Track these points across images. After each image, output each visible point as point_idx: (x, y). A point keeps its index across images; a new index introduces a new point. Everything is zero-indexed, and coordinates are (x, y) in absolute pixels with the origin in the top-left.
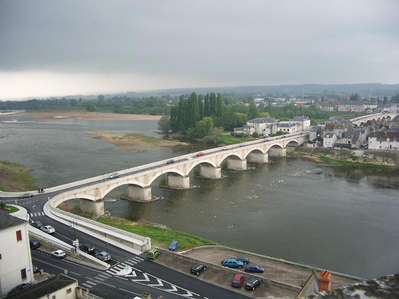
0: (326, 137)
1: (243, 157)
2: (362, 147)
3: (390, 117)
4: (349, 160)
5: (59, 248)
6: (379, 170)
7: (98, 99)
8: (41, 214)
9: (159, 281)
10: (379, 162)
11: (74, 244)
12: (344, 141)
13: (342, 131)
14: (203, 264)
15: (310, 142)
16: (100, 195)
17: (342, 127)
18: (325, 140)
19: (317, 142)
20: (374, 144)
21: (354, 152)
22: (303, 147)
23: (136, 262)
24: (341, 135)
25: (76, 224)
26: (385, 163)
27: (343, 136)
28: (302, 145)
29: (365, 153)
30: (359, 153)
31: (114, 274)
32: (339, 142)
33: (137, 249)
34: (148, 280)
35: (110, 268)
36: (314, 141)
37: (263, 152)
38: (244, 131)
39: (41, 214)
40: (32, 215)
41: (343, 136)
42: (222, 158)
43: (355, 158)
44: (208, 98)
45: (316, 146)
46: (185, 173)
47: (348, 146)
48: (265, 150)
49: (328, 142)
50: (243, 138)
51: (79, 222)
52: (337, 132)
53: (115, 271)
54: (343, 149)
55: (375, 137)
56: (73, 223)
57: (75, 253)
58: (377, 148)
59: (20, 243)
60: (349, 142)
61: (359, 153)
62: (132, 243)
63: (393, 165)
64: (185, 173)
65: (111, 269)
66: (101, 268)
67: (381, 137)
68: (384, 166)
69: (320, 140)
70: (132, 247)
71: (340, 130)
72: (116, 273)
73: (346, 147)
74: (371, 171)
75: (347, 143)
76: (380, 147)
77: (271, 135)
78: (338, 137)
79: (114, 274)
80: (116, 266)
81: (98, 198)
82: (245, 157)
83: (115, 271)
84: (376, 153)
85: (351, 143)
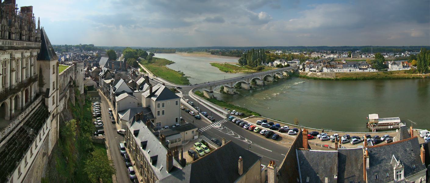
0: (306, 67)
2: (320, 71)
5: (192, 111)
7: (99, 48)
9: (239, 136)
22: (297, 72)
23: (216, 123)
25: (200, 101)
31: (213, 127)
34: (233, 134)
35: (212, 123)
39: (188, 95)
40: (184, 95)
51: (201, 100)
53: (214, 125)
56: (199, 100)
59: (177, 105)
61: (319, 74)
62: (223, 113)
64: (248, 82)
65: (212, 124)
66: (208, 123)
72: (214, 126)
74: (72, 84)
76: (350, 71)
79: (213, 127)
80: (215, 123)
83: (214, 125)
84: (326, 74)
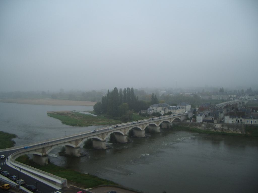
0: (198, 116)
1: (143, 128)
3: (244, 103)
4: (212, 130)
6: (95, 124)
8: (3, 164)
10: (231, 131)
11: (18, 182)
12: (210, 118)
13: (209, 112)
14: (9, 183)
15: (188, 119)
16: (46, 152)
17: (208, 110)
18: (197, 117)
19: (193, 118)
20: (229, 120)
21: (215, 125)
24: (208, 114)
26: (235, 132)
27: (209, 115)
28: (183, 121)
29: (222, 126)
30: (218, 126)
32: (206, 119)
33: (59, 186)
36: (191, 118)
37: (157, 125)
38: (149, 112)
41: (209, 115)
42: (128, 129)
43: (216, 129)
44: (125, 91)
45: (192, 121)
46: (103, 139)
47: (212, 121)
48: (158, 124)
49: (200, 119)
50: (146, 116)
52: (206, 112)
54: (209, 123)
55: (229, 115)
57: (18, 188)
58: (230, 122)
60: (212, 119)
61: (218, 126)
63: (240, 133)
64: (103, 139)
67: (232, 115)
68: (234, 134)
69: (195, 117)
70: (56, 185)
71: (207, 111)
73: (211, 122)
75: (211, 119)
76: (232, 122)
77: (165, 114)
78: (206, 116)
81: (44, 154)
82: (144, 129)
84: (229, 126)
85: (214, 119)
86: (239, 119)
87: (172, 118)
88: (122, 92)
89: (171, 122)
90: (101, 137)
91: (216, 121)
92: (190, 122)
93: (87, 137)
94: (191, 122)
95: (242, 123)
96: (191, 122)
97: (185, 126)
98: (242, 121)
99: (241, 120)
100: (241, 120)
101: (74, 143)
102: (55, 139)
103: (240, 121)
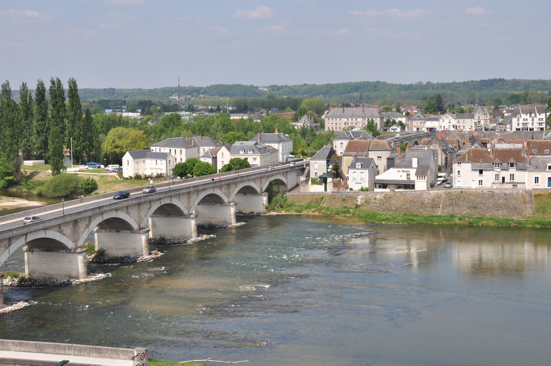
64: (75, 241)
76: (481, 182)
86: (506, 174)
87: (154, 200)
88: (45, 91)
89: (261, 189)
90: (68, 237)
91: (425, 188)
92: (323, 190)
93: (23, 235)
94: (326, 190)
95: (515, 185)
96: (326, 190)
97: (222, 281)
98: (516, 180)
99: (512, 176)
100: (512, 176)
101: (68, 230)
102: (15, 226)
103: (507, 180)
